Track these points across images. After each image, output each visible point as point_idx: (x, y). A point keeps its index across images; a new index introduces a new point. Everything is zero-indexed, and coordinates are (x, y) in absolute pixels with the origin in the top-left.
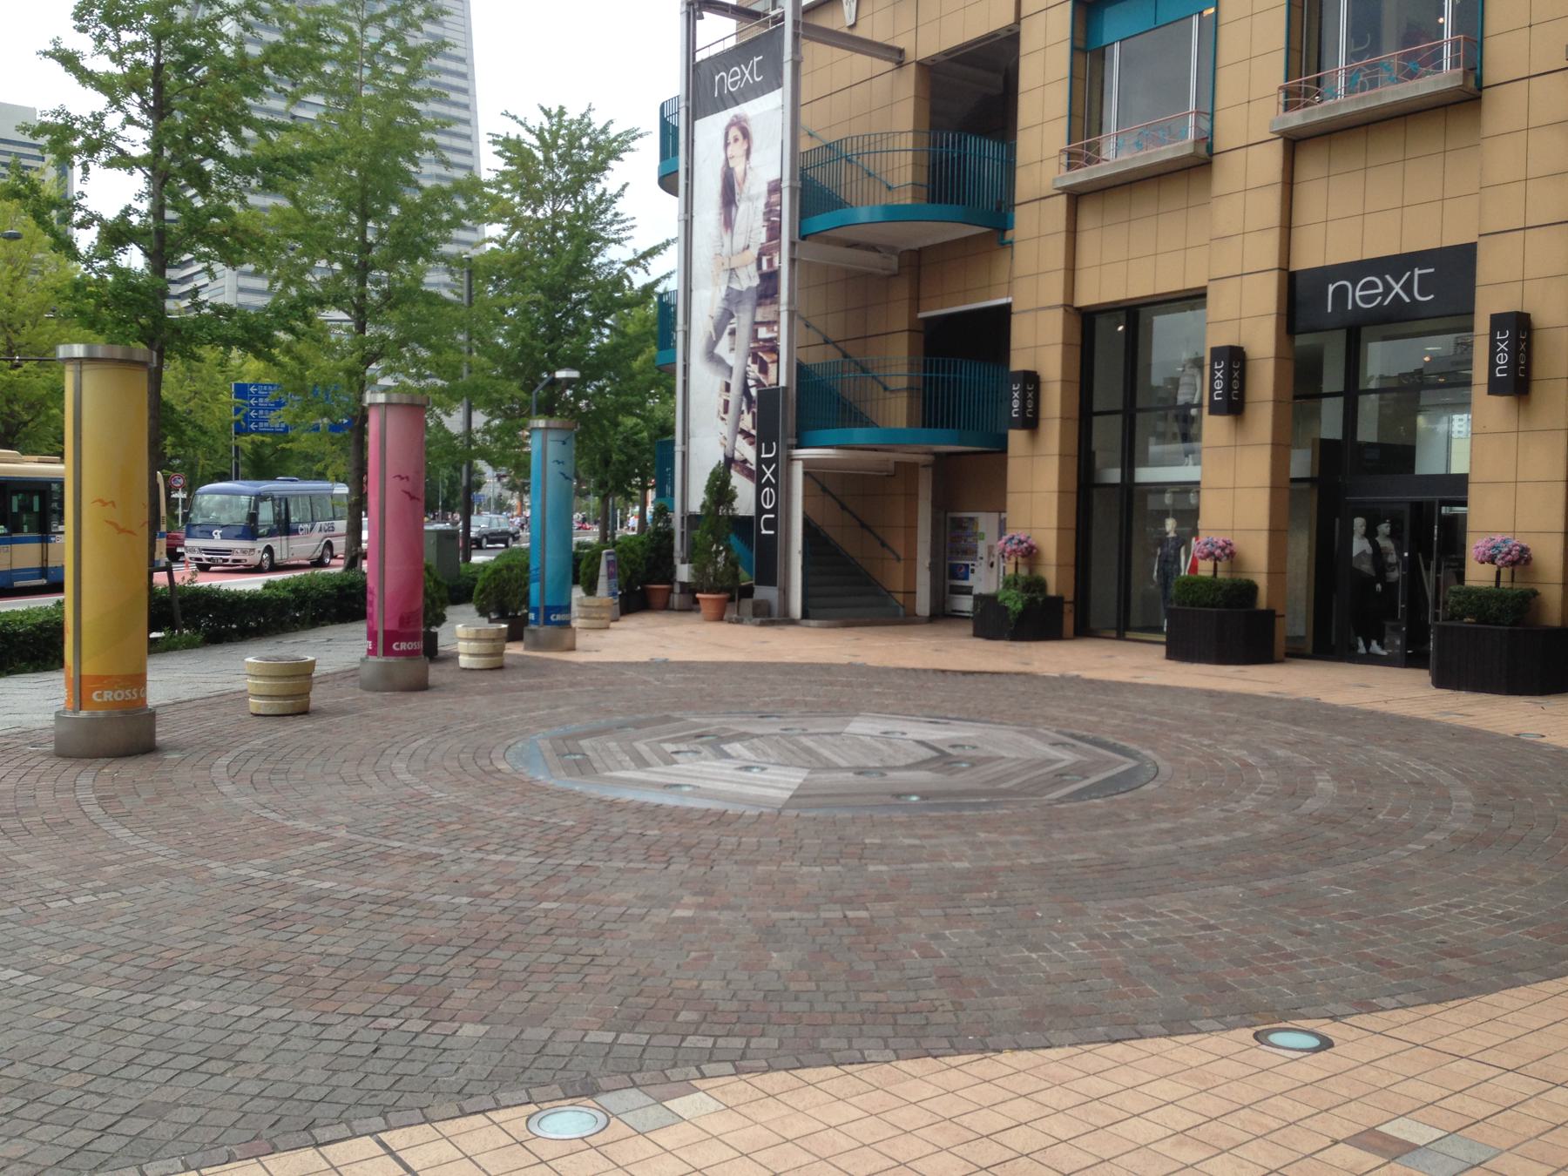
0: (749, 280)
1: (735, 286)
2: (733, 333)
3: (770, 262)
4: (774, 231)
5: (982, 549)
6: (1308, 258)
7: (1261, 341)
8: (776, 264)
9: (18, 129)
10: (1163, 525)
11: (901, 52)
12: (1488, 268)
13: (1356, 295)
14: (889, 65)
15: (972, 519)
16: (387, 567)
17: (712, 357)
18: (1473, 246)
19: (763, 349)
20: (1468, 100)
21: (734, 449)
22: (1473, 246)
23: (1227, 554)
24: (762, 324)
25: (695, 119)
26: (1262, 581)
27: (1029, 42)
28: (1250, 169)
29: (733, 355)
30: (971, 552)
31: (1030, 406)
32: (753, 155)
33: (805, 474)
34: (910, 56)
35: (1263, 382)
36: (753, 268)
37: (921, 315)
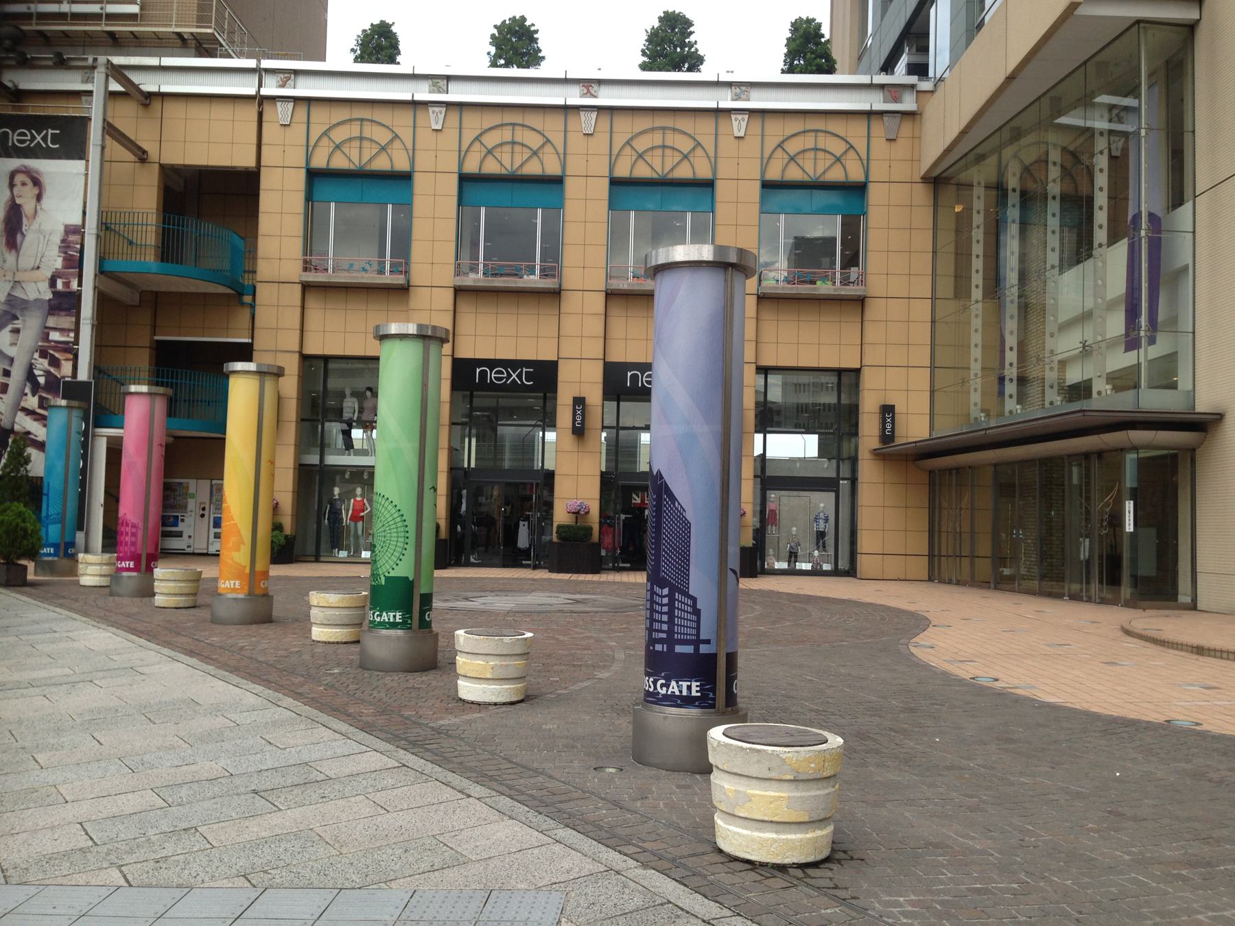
1: (18, 293)
2: (16, 331)
3: (67, 284)
4: (74, 263)
5: (191, 504)
6: (616, 356)
8: (74, 285)
9: (887, 410)
10: (333, 490)
11: (144, 152)
12: (564, 374)
13: (492, 375)
14: (131, 157)
15: (180, 484)
16: (425, 525)
19: (55, 349)
21: (13, 423)
27: (267, 181)
30: (184, 507)
31: (579, 420)
33: (108, 449)
37: (156, 338)
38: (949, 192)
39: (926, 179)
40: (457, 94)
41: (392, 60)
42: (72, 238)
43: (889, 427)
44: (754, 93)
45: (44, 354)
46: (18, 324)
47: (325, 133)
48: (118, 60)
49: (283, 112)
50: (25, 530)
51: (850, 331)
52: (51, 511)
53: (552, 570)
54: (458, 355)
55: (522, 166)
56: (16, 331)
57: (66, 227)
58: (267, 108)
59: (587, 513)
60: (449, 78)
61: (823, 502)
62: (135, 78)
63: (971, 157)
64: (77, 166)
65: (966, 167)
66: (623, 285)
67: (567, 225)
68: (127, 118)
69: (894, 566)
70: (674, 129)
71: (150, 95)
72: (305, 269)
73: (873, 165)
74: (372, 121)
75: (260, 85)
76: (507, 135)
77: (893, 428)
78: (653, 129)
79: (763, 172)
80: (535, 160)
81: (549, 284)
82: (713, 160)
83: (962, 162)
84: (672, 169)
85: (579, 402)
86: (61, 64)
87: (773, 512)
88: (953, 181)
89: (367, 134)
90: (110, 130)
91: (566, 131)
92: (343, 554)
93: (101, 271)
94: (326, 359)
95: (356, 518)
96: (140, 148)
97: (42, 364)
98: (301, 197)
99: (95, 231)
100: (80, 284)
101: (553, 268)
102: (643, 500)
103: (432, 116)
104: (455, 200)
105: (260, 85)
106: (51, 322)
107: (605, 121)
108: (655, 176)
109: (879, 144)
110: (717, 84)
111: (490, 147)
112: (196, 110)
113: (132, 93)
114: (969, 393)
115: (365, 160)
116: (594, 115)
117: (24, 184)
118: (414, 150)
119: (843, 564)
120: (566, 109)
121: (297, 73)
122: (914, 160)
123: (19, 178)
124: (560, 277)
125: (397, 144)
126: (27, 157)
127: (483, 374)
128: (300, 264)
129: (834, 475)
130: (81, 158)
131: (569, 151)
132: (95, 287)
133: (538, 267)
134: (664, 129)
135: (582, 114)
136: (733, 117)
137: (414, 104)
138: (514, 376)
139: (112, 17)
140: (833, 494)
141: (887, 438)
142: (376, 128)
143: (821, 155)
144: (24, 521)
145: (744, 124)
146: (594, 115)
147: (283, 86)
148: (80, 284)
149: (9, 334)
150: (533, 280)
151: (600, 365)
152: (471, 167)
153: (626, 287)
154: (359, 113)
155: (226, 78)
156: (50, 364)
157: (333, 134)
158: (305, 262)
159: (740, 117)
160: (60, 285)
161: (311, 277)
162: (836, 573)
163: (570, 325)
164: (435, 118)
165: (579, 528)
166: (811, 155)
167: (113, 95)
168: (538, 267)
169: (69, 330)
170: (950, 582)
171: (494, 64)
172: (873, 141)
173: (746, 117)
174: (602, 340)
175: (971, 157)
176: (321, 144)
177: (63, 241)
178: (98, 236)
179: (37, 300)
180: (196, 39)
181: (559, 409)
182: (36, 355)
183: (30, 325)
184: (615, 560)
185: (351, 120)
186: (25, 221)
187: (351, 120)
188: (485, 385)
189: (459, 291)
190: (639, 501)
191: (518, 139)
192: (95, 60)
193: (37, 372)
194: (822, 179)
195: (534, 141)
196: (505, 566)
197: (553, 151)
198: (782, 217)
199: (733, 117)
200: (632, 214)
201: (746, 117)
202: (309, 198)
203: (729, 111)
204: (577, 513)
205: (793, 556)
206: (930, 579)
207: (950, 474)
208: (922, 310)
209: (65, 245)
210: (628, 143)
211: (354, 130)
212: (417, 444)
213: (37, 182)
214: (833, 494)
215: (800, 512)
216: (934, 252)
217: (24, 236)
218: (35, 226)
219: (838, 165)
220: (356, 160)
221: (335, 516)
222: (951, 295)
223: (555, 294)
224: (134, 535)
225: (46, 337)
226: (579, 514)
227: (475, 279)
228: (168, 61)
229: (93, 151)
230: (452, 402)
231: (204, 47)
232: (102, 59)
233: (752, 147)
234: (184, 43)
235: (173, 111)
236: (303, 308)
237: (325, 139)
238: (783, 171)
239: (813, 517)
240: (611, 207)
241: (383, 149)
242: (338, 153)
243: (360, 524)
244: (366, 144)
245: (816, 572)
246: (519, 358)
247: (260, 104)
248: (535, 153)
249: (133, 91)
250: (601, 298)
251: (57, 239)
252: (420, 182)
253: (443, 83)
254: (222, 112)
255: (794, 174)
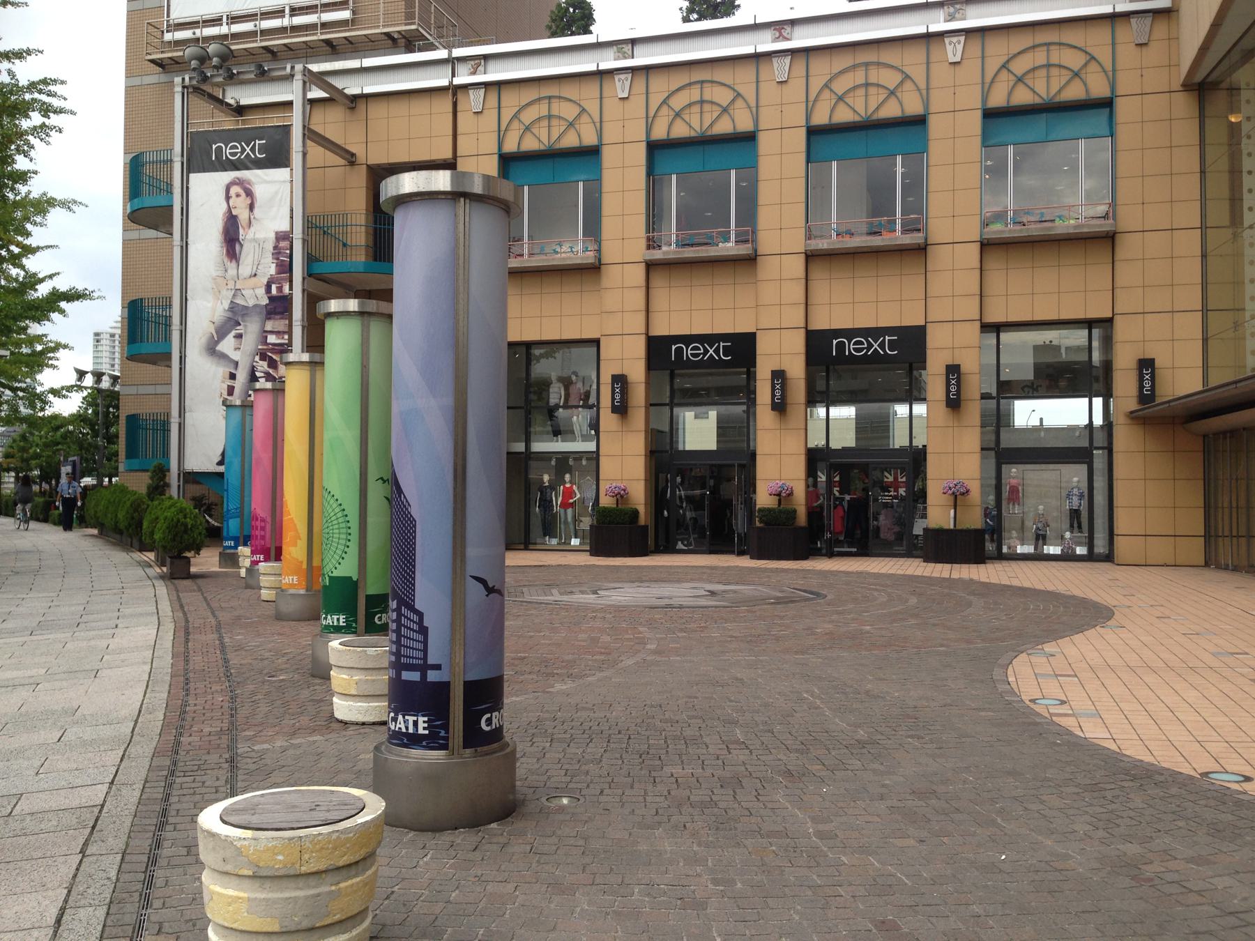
0: (256, 296)
1: (239, 301)
2: (239, 336)
3: (280, 289)
4: (285, 268)
6: (660, 330)
7: (637, 372)
8: (286, 290)
9: (1146, 365)
11: (353, 155)
12: (762, 346)
13: (850, 348)
14: (343, 162)
17: (212, 349)
18: (754, 335)
19: (272, 351)
20: (750, 260)
22: (754, 335)
23: (621, 496)
24: (271, 332)
25: (189, 172)
26: (641, 509)
28: (624, 278)
29: (239, 353)
31: (953, 389)
32: (256, 211)
34: (361, 157)
35: (638, 395)
36: (261, 291)
38: (1219, 100)
39: (1187, 86)
40: (643, 58)
41: (587, 31)
42: (283, 244)
43: (1147, 385)
44: (799, 31)
45: (263, 357)
46: (240, 330)
47: (665, 102)
48: (315, 68)
49: (475, 99)
50: (186, 525)
51: (1098, 275)
52: (231, 507)
53: (927, 559)
54: (812, 327)
55: (1059, 91)
56: (239, 336)
57: (277, 233)
58: (460, 96)
59: (791, 494)
60: (633, 42)
61: (1075, 475)
62: (338, 83)
63: (1235, 56)
64: (281, 174)
65: (1233, 68)
66: (822, 244)
67: (932, 170)
68: (331, 123)
69: (1159, 549)
70: (878, 64)
71: (355, 98)
72: (649, 247)
73: (606, 126)
74: (560, 97)
75: (453, 75)
76: (695, 94)
77: (1153, 386)
78: (854, 67)
79: (985, 99)
80: (726, 118)
81: (744, 250)
82: (754, 110)
83: (1226, 63)
84: (877, 108)
85: (779, 376)
86: (263, 76)
87: (1014, 490)
88: (1223, 85)
89: (555, 112)
90: (310, 134)
91: (983, 58)
92: (554, 541)
93: (309, 274)
94: (528, 345)
95: (565, 505)
96: (347, 152)
97: (263, 366)
98: (642, 172)
99: (300, 236)
100: (291, 289)
101: (918, 221)
102: (896, 478)
103: (618, 84)
104: (803, 157)
105: (453, 75)
106: (269, 326)
107: (975, 47)
108: (857, 119)
109: (1127, 54)
110: (756, 27)
111: (677, 109)
112: (399, 109)
113: (336, 98)
114: (1244, 339)
115: (706, 125)
116: (788, 60)
117: (238, 195)
118: (757, 107)
119: (1100, 547)
120: (757, 57)
121: (486, 57)
122: (1172, 65)
123: (235, 190)
124: (754, 241)
125: (585, 118)
126: (238, 169)
127: (679, 350)
128: (643, 243)
129: (1086, 444)
130: (287, 166)
131: (762, 103)
132: (304, 290)
133: (899, 222)
134: (867, 64)
135: (775, 60)
136: (947, 41)
137: (600, 74)
138: (711, 351)
139: (264, 32)
140: (1085, 467)
141: (1146, 398)
142: (564, 104)
143: (1054, 71)
144: (185, 517)
145: (960, 48)
146: (788, 60)
147: (474, 73)
148: (291, 289)
149: (233, 340)
150: (729, 247)
151: (802, 333)
152: (659, 133)
153: (825, 246)
154: (698, 75)
155: (712, 41)
156: (269, 366)
157: (672, 102)
158: (648, 239)
159: (955, 40)
160: (274, 291)
161: (657, 255)
162: (1091, 557)
163: (938, 284)
164: (621, 86)
165: (780, 511)
166: (1043, 72)
167: (313, 102)
168: (899, 222)
169: (284, 333)
170: (1226, 568)
171: (686, 20)
172: (1119, 48)
173: (962, 39)
174: (802, 307)
175: (1235, 56)
176: (660, 114)
177: (275, 248)
178: (304, 240)
179: (256, 306)
180: (404, 37)
181: (758, 384)
182: (257, 358)
183: (251, 329)
184: (839, 543)
185: (690, 84)
186: (241, 231)
187: (690, 84)
188: (681, 362)
189: (650, 266)
190: (891, 479)
191: (707, 97)
192: (293, 68)
193: (258, 374)
194: (1057, 99)
195: (723, 96)
196: (711, 552)
197: (744, 105)
198: (1082, 144)
199: (947, 41)
200: (834, 164)
201: (962, 39)
202: (650, 171)
203: (941, 35)
204: (779, 495)
205: (1041, 538)
206: (1207, 565)
207: (1225, 438)
208: (1190, 243)
209: (277, 251)
210: (1004, 66)
211: (543, 109)
212: (357, 432)
213: (249, 193)
214: (1085, 467)
215: (1047, 490)
216: (1203, 172)
217: (241, 246)
218: (250, 235)
219: (1077, 80)
220: (545, 140)
221: (546, 504)
222: (1227, 223)
223: (921, 250)
224: (263, 529)
225: (265, 342)
226: (783, 496)
227: (670, 250)
228: (369, 62)
229: (296, 159)
230: (647, 383)
231: (409, 42)
232: (299, 67)
233: (971, 71)
234: (394, 42)
235: (377, 111)
236: (648, 288)
237: (665, 108)
238: (1010, 94)
239: (1064, 494)
240: (985, 143)
241: (571, 125)
242: (679, 122)
243: (570, 511)
244: (707, 107)
245: (1067, 557)
246: (880, 325)
247: (454, 94)
248: (725, 110)
249: (336, 96)
250: (976, 248)
251: (270, 247)
252: (765, 142)
253: (627, 48)
254: (420, 106)
255: (1023, 97)
